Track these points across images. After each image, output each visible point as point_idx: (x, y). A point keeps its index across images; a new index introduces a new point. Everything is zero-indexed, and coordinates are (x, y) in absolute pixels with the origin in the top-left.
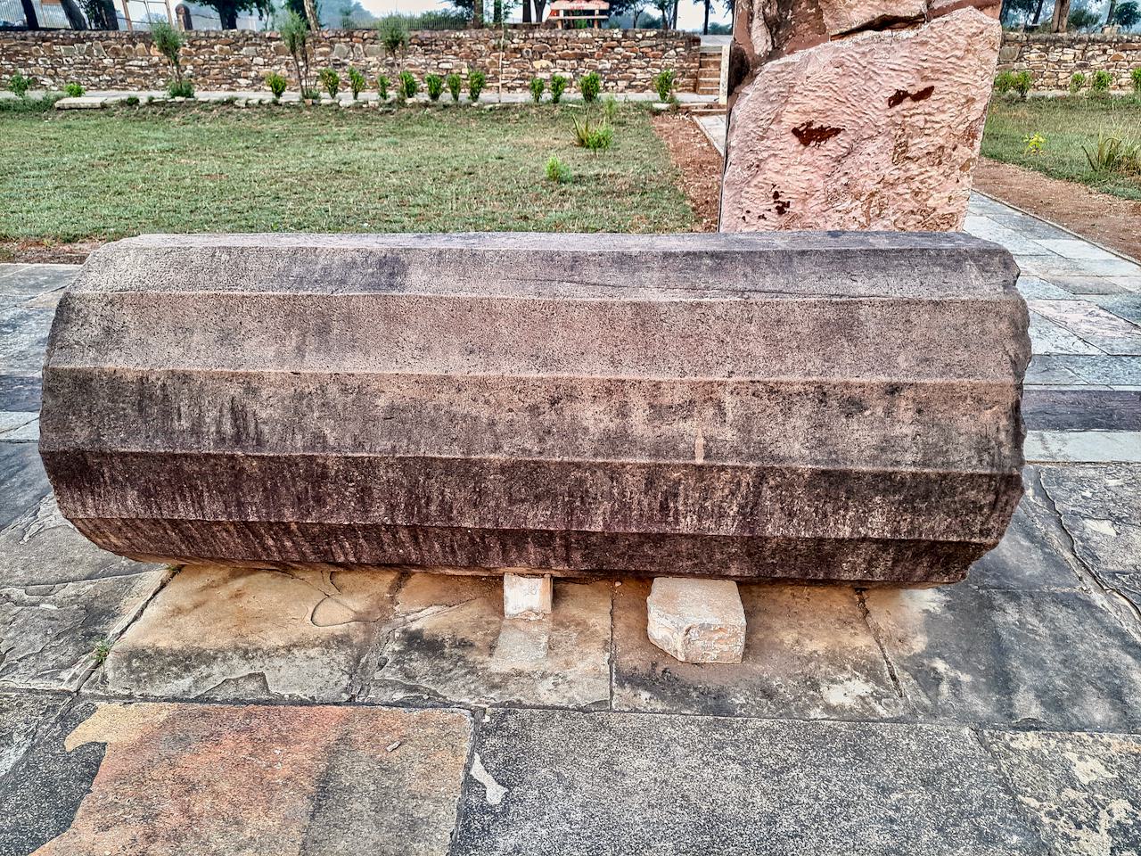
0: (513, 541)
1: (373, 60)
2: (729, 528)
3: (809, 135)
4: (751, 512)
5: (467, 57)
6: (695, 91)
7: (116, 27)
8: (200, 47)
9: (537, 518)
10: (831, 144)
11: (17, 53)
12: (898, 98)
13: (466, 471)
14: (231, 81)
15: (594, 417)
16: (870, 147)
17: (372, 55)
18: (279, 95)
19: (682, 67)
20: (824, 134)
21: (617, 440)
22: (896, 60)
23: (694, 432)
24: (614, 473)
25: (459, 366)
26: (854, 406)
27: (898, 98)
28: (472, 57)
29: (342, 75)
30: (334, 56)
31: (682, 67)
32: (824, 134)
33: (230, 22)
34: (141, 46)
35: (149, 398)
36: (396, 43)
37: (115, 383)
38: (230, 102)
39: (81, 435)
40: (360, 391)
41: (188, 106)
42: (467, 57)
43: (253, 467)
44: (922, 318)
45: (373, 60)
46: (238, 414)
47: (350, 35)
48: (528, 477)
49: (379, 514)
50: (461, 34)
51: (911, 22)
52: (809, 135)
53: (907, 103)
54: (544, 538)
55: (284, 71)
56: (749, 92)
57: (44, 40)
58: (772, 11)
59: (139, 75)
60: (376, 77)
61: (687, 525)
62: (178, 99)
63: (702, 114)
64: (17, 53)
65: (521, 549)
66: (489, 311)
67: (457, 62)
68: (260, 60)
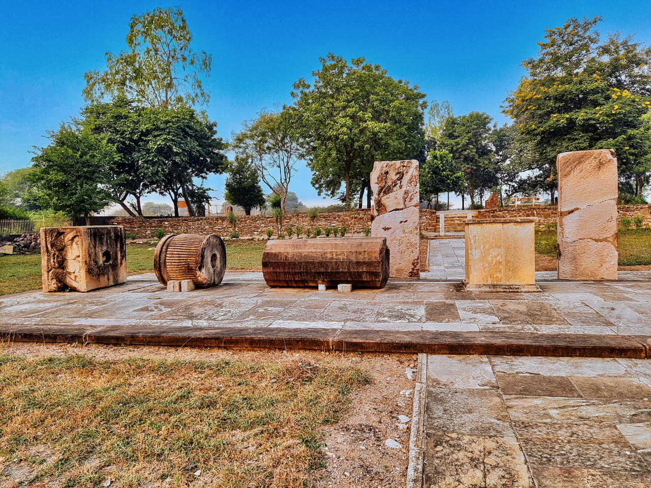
0: (319, 273)
1: (306, 224)
2: (346, 270)
3: (386, 229)
4: (349, 268)
5: (341, 221)
6: (435, 232)
7: (204, 215)
8: (242, 221)
9: (322, 270)
10: (390, 230)
11: (175, 225)
12: (401, 222)
13: (313, 263)
14: (252, 233)
15: (329, 256)
16: (398, 231)
17: (305, 222)
18: (270, 236)
19: (429, 223)
20: (388, 229)
21: (332, 258)
22: (400, 216)
23: (341, 257)
24: (331, 262)
25: (313, 250)
26: (360, 253)
27: (401, 222)
28: (343, 221)
29: (294, 229)
30: (291, 223)
31: (429, 223)
32: (388, 229)
33: (248, 213)
34: (220, 221)
35: (276, 255)
36: (314, 217)
37: (272, 253)
38: (252, 239)
39: (267, 260)
40: (301, 253)
41: (237, 241)
42: (341, 221)
43: (287, 263)
44: (369, 244)
45: (306, 224)
46: (286, 257)
47: (298, 215)
48: (321, 264)
49: (302, 270)
50: (340, 214)
51: (402, 209)
52: (386, 229)
53: (403, 223)
54: (323, 273)
55: (272, 229)
56: (374, 222)
57: (186, 220)
58: (377, 208)
59: (218, 232)
60: (306, 230)
61: (341, 270)
62: (234, 239)
63: (432, 239)
64: (175, 225)
65: (320, 275)
66: (317, 244)
67: (338, 223)
68: (263, 225)
